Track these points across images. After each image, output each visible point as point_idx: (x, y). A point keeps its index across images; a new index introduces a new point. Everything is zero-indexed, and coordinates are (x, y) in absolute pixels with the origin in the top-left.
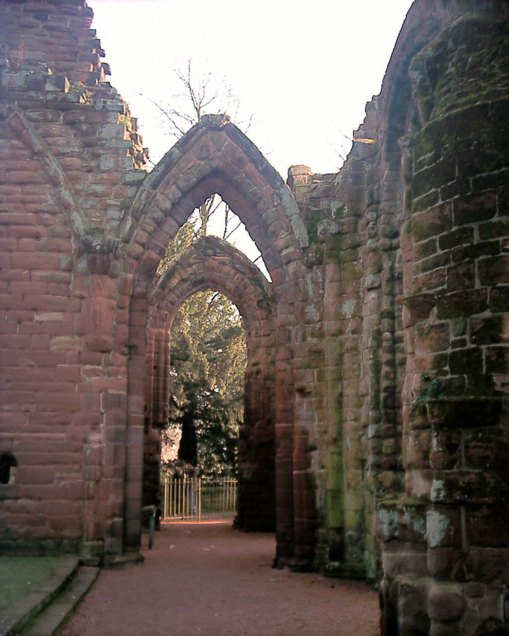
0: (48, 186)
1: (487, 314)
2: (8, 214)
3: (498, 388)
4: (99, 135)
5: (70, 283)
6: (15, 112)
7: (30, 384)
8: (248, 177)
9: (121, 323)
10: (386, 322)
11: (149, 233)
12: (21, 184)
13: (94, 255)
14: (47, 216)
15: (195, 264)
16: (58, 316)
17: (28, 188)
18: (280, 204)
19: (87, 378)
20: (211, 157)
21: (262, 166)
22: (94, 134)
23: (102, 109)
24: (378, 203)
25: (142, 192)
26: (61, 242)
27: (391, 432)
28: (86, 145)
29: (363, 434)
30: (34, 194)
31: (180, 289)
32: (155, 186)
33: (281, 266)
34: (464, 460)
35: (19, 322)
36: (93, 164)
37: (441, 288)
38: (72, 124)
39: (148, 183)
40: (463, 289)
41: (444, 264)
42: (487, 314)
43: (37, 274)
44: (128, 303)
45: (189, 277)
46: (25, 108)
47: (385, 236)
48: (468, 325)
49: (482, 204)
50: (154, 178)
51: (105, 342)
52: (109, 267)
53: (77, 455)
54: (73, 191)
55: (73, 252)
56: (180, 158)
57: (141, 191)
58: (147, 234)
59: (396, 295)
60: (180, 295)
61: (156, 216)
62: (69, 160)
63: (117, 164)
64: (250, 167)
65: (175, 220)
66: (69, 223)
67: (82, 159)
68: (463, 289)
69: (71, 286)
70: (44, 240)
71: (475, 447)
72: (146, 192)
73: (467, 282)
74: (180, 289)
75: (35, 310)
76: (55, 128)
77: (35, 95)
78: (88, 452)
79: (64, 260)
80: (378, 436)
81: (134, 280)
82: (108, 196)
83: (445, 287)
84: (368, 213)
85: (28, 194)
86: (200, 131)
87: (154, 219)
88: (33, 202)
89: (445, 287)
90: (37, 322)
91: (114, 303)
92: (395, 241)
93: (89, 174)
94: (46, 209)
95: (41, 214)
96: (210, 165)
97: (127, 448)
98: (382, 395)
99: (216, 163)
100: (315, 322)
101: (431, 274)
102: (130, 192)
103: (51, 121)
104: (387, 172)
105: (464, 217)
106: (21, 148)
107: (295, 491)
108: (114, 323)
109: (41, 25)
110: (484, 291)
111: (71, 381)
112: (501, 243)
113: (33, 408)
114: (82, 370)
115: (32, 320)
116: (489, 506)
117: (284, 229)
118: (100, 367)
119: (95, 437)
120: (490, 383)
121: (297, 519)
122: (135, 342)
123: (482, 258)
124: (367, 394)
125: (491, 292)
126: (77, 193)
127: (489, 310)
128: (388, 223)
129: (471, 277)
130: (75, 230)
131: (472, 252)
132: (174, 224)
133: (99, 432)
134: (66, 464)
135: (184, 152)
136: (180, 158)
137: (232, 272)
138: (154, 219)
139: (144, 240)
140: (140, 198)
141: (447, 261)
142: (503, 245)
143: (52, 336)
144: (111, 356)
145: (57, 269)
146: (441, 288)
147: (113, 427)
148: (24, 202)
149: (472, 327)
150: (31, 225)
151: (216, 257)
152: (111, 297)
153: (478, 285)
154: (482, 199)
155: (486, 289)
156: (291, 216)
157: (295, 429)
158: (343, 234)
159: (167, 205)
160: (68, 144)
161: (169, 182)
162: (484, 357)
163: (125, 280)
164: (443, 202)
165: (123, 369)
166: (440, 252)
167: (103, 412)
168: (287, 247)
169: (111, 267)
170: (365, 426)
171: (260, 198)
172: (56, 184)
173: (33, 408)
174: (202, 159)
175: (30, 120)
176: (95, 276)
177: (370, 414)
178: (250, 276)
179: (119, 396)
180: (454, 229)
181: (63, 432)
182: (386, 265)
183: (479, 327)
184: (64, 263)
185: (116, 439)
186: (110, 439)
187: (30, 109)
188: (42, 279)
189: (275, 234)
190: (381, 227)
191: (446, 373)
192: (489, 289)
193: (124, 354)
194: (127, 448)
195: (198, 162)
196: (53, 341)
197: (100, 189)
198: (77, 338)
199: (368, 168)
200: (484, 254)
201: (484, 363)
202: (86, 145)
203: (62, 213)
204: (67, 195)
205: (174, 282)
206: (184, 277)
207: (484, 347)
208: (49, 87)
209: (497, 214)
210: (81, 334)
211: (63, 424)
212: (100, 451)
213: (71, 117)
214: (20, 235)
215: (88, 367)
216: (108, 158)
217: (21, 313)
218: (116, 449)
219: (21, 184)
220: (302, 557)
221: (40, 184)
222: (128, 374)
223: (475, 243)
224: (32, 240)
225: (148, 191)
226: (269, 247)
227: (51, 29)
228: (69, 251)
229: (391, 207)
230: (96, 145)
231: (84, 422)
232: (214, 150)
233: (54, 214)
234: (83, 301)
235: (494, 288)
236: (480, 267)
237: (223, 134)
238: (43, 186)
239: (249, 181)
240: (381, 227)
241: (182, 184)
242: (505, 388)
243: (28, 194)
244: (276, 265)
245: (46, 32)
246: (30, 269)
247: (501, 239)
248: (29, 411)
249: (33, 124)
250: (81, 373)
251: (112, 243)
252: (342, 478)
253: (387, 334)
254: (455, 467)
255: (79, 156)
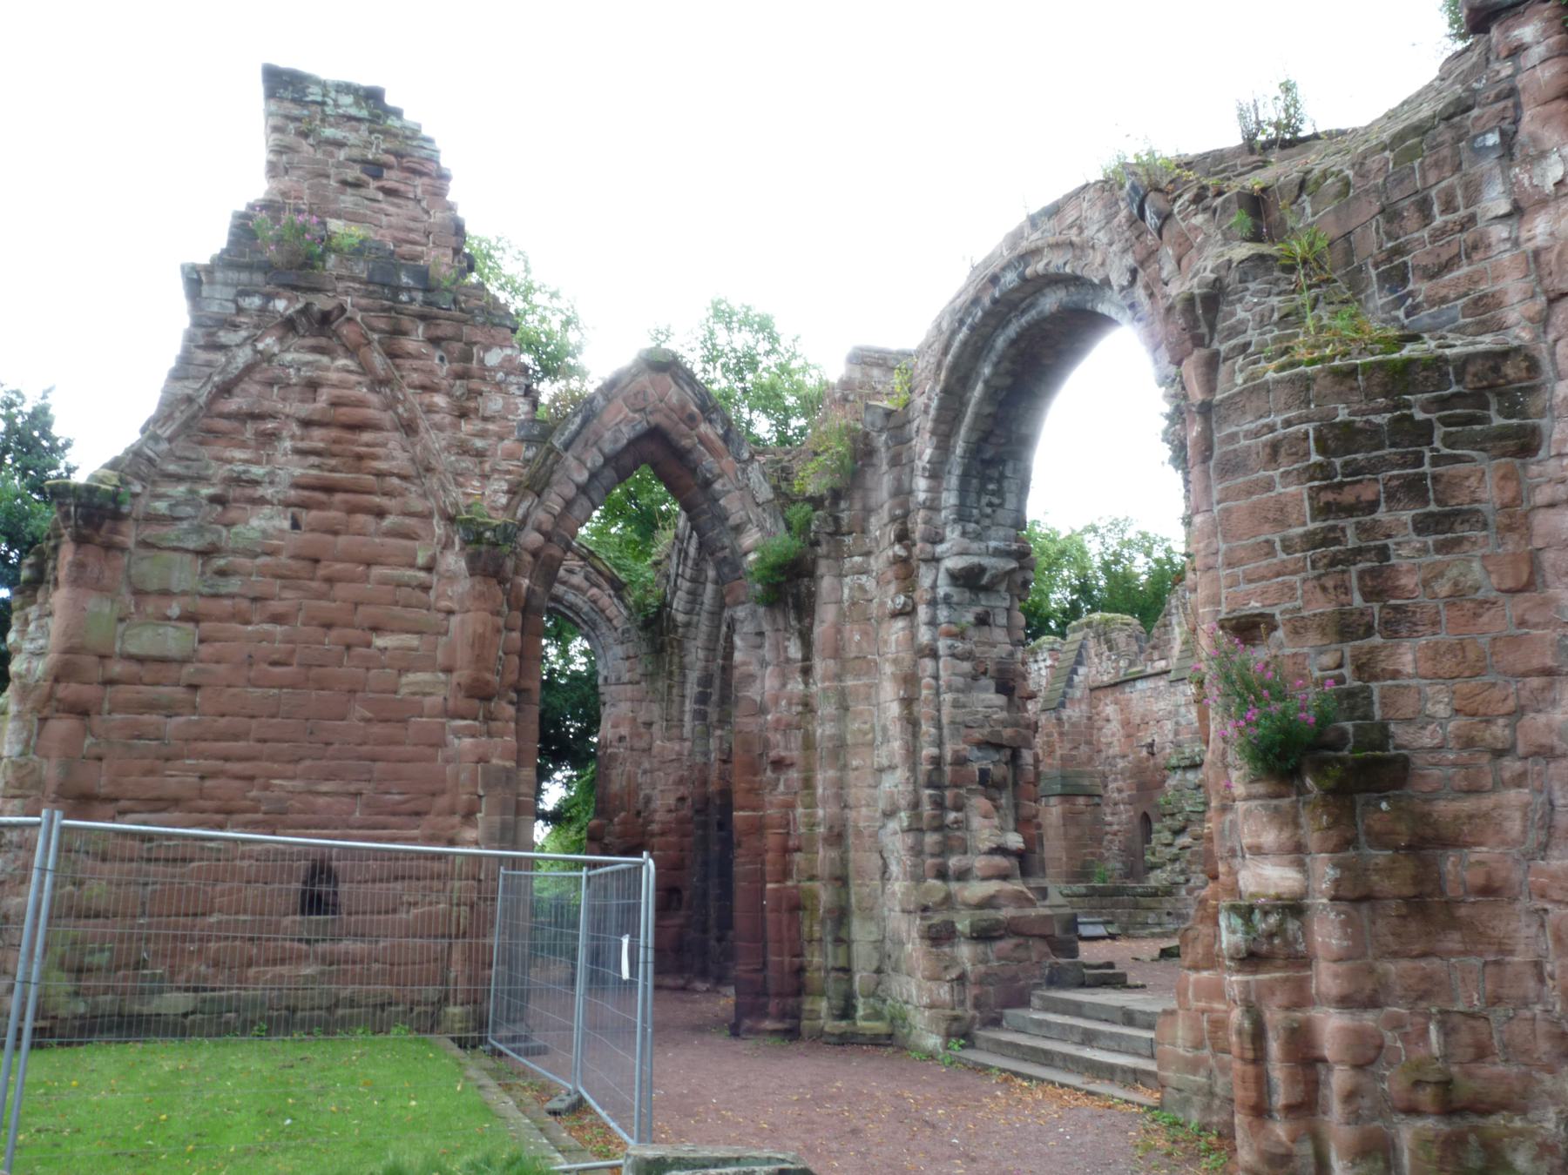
7: (365, 748)
8: (701, 441)
14: (395, 481)
16: (412, 640)
43: (377, 571)
51: (488, 683)
75: (376, 629)
107: (770, 916)
109: (373, 184)
111: (432, 745)
115: (369, 645)
121: (773, 958)
123: (1361, 566)
129: (1347, 591)
133: (476, 826)
139: (547, 526)
143: (402, 671)
145: (412, 566)
150: (370, 493)
159: (582, 477)
165: (512, 725)
173: (366, 788)
174: (636, 411)
179: (505, 769)
181: (417, 827)
188: (384, 582)
193: (511, 703)
196: (404, 680)
198: (442, 676)
210: (448, 670)
211: (418, 814)
217: (352, 634)
220: (782, 1016)
227: (390, 192)
231: (452, 812)
245: (380, 196)
246: (369, 565)
252: (848, 894)
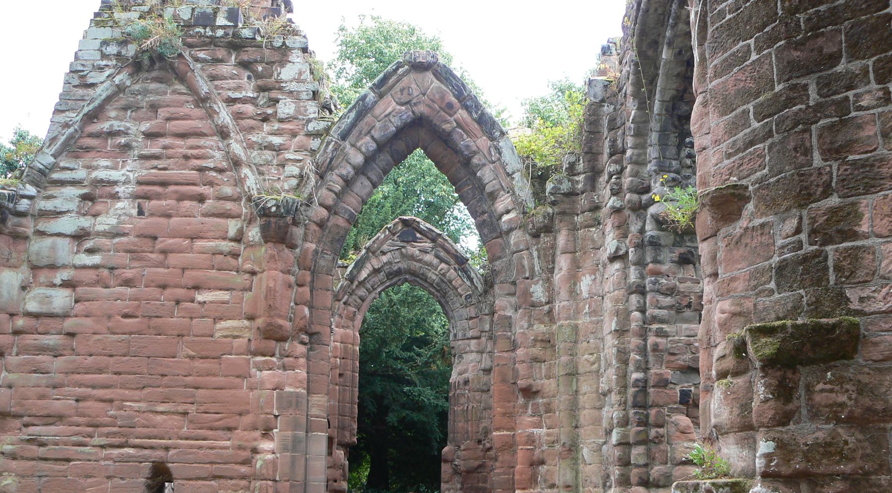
0: (215, 138)
1: (834, 200)
2: (167, 172)
3: (855, 305)
4: (278, 76)
5: (239, 255)
6: (179, 51)
7: (189, 379)
8: (459, 125)
9: (301, 304)
10: (634, 299)
11: (336, 193)
12: (183, 136)
13: (268, 219)
15: (390, 251)
16: (224, 296)
17: (192, 141)
18: (499, 159)
19: (258, 372)
20: (414, 101)
21: (476, 113)
22: (271, 76)
23: (282, 46)
24: (624, 152)
25: (328, 144)
26: (229, 205)
27: (642, 437)
28: (262, 89)
29: (605, 443)
30: (198, 147)
31: (371, 282)
32: (344, 136)
33: (500, 236)
34: (804, 412)
35: (178, 302)
36: (270, 111)
37: (758, 174)
38: (245, 65)
39: (335, 132)
40: (796, 168)
41: (764, 139)
42: (834, 200)
43: (199, 243)
44: (309, 279)
45: (382, 267)
46: (190, 46)
47: (632, 190)
48: (805, 219)
49: (821, 49)
50: (343, 126)
51: (280, 327)
52: (286, 233)
53: (244, 469)
54: (245, 144)
55: (243, 217)
56: (376, 102)
57: (327, 142)
58: (334, 196)
59: (647, 264)
60: (371, 289)
61: (344, 172)
62: (238, 107)
63: (297, 110)
64: (462, 114)
65: (368, 178)
66: (240, 182)
67: (256, 105)
68: (796, 168)
69: (240, 260)
70: (209, 202)
71: (822, 391)
72: (333, 143)
73: (801, 159)
74: (371, 282)
75: (197, 288)
76: (226, 69)
77: (202, 31)
78: (258, 466)
79: (233, 227)
80: (624, 444)
81: (316, 252)
82: (286, 149)
83: (766, 171)
84: (609, 165)
85: (191, 148)
86: (401, 71)
87: (341, 176)
88: (197, 158)
89: (766, 171)
90: (200, 303)
91: (292, 279)
92: (645, 197)
93: (265, 124)
94: (212, 165)
95: (207, 172)
96: (413, 112)
97: (306, 460)
98: (631, 391)
99: (421, 109)
100: (541, 304)
101: (743, 158)
102: (315, 143)
103: (221, 61)
104: (635, 113)
105: (792, 69)
106: (185, 94)
108: (292, 304)
110: (828, 169)
112: (851, 98)
113: (192, 409)
114: (251, 362)
115: (192, 301)
116: (845, 477)
117: (504, 190)
118: (274, 359)
119: (266, 445)
120: (841, 299)
122: (315, 328)
124: (610, 391)
125: (839, 169)
126: (251, 146)
127: (835, 194)
128: (635, 174)
130: (247, 190)
131: (804, 122)
132: (367, 183)
133: (272, 439)
134: (231, 479)
135: (381, 96)
136: (376, 102)
137: (436, 261)
138: (341, 176)
139: (330, 202)
140: (325, 151)
141: (770, 134)
142: (856, 102)
143: (216, 320)
144: (287, 345)
145: (224, 239)
146: (758, 174)
147: (289, 433)
148: (186, 157)
149: (813, 220)
151: (415, 244)
152: (289, 272)
153: (817, 160)
154: (820, 41)
155: (831, 166)
156: (514, 173)
157: (518, 439)
158: (578, 194)
159: (358, 159)
160: (239, 88)
161: (361, 132)
162: (830, 263)
163: (305, 252)
164: (758, 56)
165: (302, 361)
166: (756, 125)
167: (277, 414)
168: (508, 212)
169: (289, 234)
170: (609, 433)
171: (475, 153)
172: (224, 134)
173: (192, 409)
174: (402, 104)
175: (197, 60)
176: (270, 244)
177: (614, 415)
178: (457, 266)
179: (297, 395)
180: (778, 88)
182: (634, 228)
183: (821, 220)
184: (232, 232)
185: (294, 449)
186: (285, 449)
187: (198, 47)
189: (493, 196)
190: (627, 181)
191: (772, 292)
192: (835, 166)
193: (303, 343)
194: (306, 460)
195: (398, 107)
196: (218, 326)
197: (277, 140)
199: (607, 109)
200: (827, 117)
201: (831, 270)
202: (262, 89)
203: (231, 171)
204: (237, 148)
205: (364, 274)
206: (376, 267)
207: (829, 248)
208: (221, 21)
209: (843, 60)
210: (251, 318)
211: (230, 429)
212: (274, 463)
213: (245, 57)
214: (182, 198)
215: (259, 359)
216: (287, 104)
217: (180, 292)
218: (293, 460)
219: (183, 136)
221: (207, 136)
222: (308, 367)
223: (811, 103)
224: (194, 203)
225: (336, 142)
226: (484, 213)
228: (239, 216)
229: (639, 155)
230: (274, 88)
232: (418, 93)
233: (221, 171)
234: (254, 278)
235: (845, 162)
236: (820, 136)
237: (429, 75)
238: (210, 138)
239: (460, 131)
240: (627, 181)
241: (377, 134)
242: (864, 305)
243: (191, 148)
244: (494, 235)
247: (850, 94)
248: (188, 413)
249: (199, 65)
250: (251, 366)
251: (291, 204)
253: (637, 314)
254: (791, 423)
255: (252, 101)
